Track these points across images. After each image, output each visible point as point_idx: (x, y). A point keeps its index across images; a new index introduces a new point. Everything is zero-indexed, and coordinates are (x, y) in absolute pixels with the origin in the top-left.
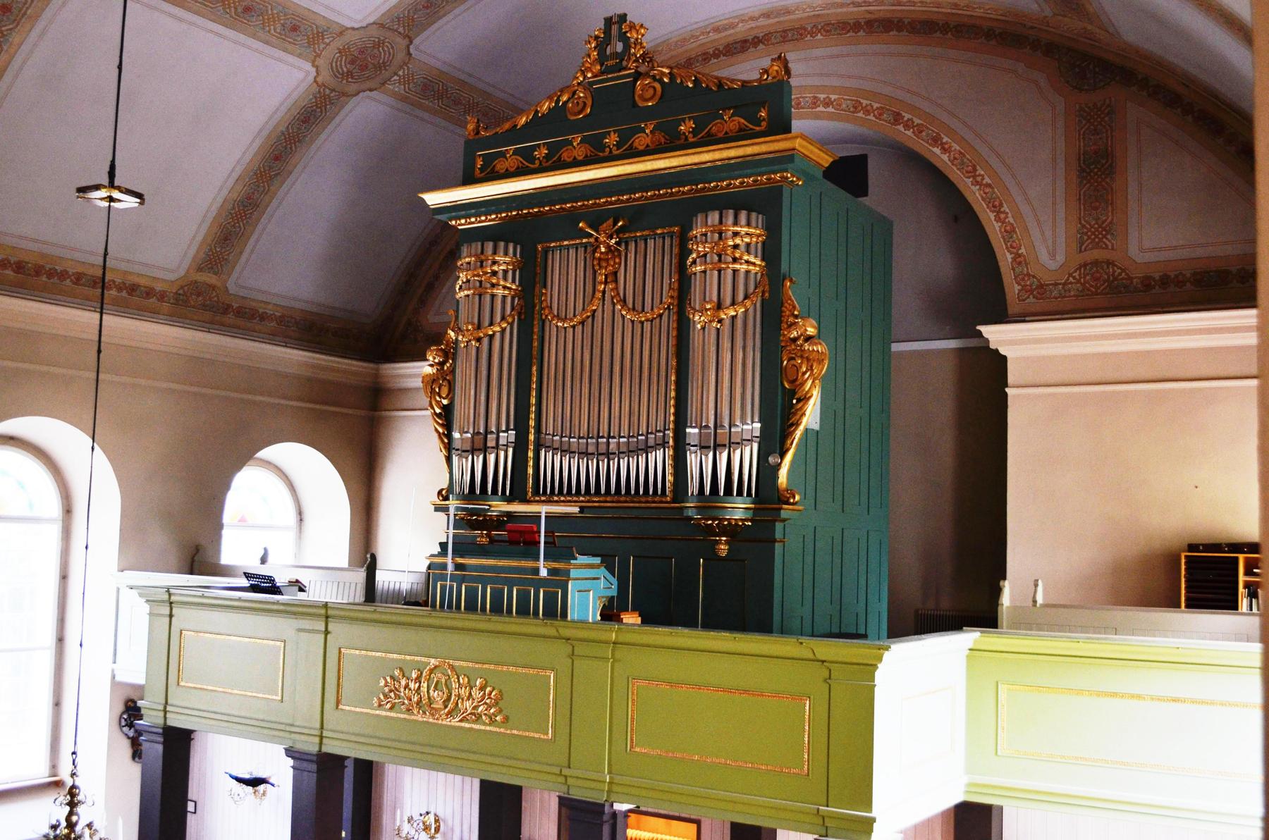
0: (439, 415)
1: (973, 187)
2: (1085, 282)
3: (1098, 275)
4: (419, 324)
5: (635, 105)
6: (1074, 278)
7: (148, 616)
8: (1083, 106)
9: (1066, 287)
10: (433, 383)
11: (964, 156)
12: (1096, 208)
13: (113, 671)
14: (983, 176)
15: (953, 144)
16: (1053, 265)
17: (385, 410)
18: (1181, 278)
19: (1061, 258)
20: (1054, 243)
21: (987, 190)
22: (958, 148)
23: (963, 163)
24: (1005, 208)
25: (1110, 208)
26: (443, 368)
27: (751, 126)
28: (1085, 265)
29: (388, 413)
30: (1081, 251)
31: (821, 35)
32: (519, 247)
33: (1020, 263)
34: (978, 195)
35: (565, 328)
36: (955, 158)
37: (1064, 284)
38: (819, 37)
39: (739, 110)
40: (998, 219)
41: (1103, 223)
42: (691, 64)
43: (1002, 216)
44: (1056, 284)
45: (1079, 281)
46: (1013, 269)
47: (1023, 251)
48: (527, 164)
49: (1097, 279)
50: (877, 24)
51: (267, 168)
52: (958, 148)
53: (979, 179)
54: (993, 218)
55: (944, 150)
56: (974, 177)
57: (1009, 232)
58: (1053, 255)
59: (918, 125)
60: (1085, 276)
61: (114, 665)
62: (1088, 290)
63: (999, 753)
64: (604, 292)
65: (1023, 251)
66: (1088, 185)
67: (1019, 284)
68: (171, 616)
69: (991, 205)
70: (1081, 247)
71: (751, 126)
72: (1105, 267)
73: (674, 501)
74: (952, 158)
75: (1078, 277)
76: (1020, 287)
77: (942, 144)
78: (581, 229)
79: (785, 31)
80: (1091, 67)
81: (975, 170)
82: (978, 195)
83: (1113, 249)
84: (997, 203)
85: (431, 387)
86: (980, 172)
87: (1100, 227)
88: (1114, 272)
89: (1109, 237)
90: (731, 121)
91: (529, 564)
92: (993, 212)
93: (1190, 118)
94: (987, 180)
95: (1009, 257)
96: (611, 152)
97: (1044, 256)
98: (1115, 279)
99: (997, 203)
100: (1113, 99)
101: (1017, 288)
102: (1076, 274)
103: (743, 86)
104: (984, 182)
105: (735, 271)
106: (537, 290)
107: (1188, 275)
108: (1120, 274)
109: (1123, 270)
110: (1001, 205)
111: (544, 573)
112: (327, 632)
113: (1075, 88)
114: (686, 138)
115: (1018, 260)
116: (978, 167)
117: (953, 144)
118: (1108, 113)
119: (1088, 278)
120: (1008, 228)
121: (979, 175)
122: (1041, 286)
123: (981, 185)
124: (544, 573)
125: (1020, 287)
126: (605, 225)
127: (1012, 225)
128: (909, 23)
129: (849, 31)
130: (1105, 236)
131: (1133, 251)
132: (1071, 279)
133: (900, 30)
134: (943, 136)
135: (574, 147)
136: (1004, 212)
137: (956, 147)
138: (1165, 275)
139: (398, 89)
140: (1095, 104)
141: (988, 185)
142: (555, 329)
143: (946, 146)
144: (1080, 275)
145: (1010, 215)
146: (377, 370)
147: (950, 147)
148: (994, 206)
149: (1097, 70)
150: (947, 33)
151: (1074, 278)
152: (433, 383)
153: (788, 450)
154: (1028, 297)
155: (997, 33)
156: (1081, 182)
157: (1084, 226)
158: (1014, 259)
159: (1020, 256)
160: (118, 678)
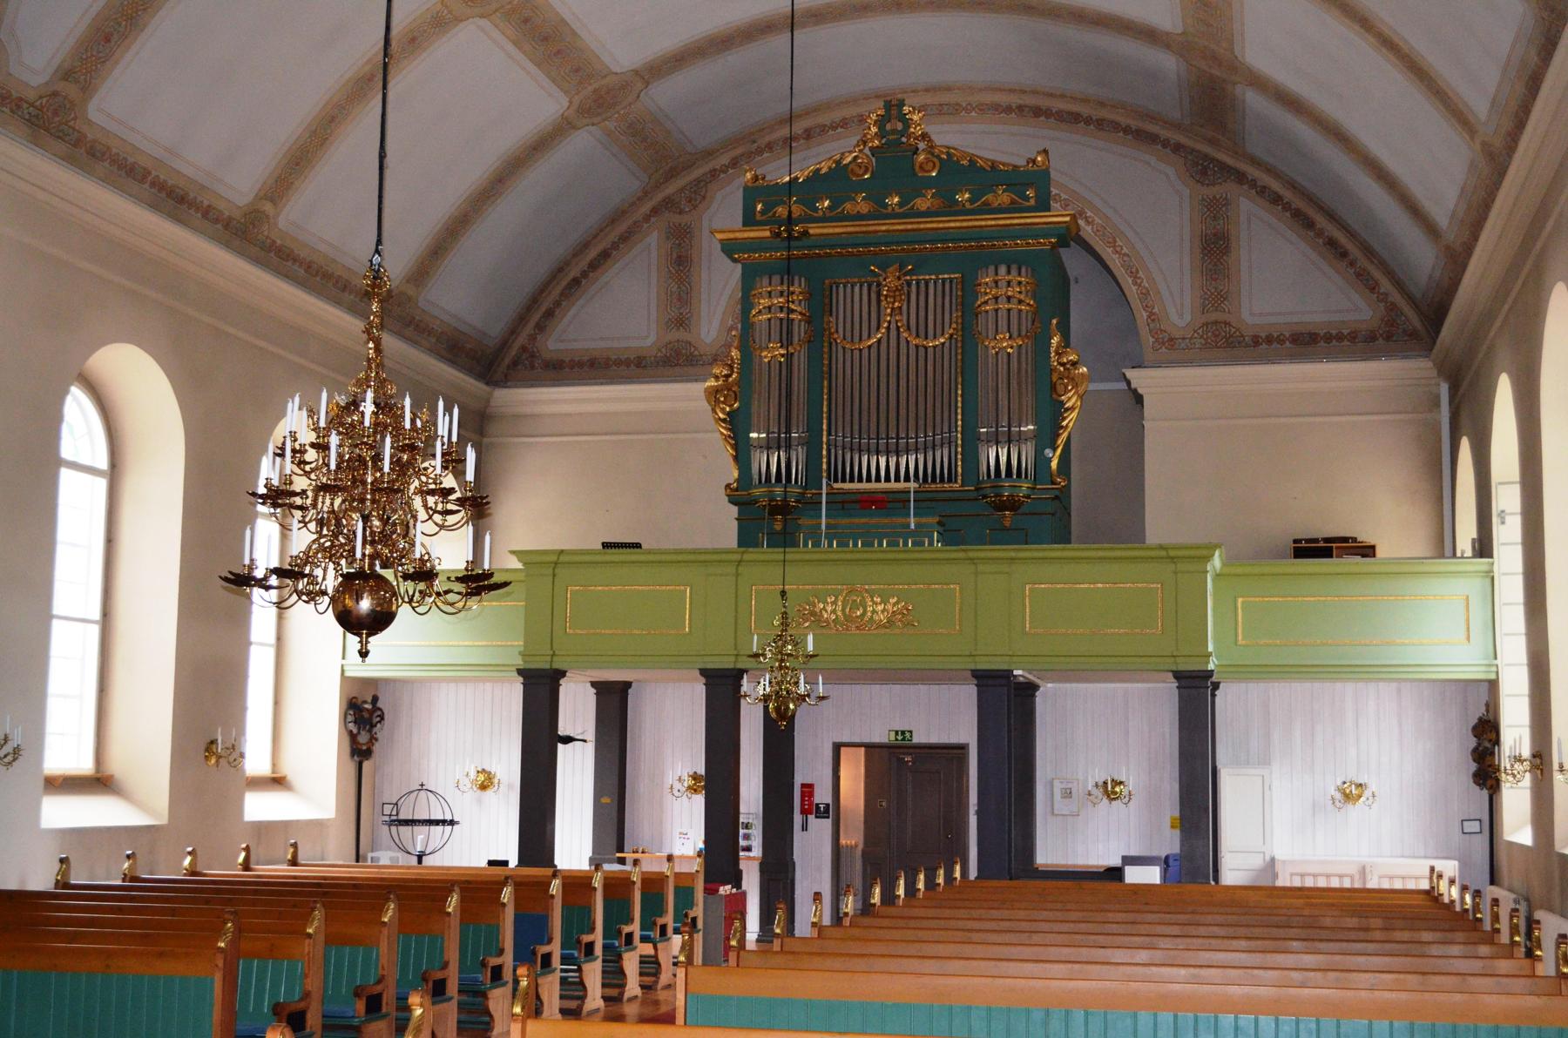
0: (724, 421)
1: (1114, 256)
2: (1208, 338)
3: (1217, 333)
4: (535, 350)
5: (915, 174)
6: (1198, 334)
7: (736, 522)
8: (1205, 197)
9: (1192, 341)
10: (716, 393)
11: (1105, 229)
12: (1215, 280)
13: (342, 666)
14: (1121, 247)
15: (1096, 218)
16: (1181, 323)
17: (511, 436)
18: (1282, 337)
19: (1188, 317)
20: (1182, 305)
21: (1125, 259)
22: (1100, 222)
23: (1104, 235)
24: (1141, 274)
25: (1227, 280)
26: (727, 381)
27: (1020, 201)
28: (1207, 324)
29: (501, 439)
30: (1203, 313)
31: (976, 112)
32: (803, 279)
33: (1153, 320)
34: (1117, 261)
35: (852, 350)
36: (1098, 231)
37: (1191, 338)
38: (973, 114)
39: (1010, 186)
40: (1135, 283)
41: (1221, 291)
42: (846, 124)
43: (1139, 281)
44: (1184, 339)
45: (1202, 337)
46: (1148, 325)
47: (1156, 310)
48: (809, 212)
49: (1216, 336)
50: (1027, 109)
51: (1218, 263)
52: (1100, 222)
53: (1118, 249)
54: (1130, 281)
55: (1088, 223)
56: (1114, 247)
57: (1145, 294)
58: (1181, 316)
59: (1065, 199)
60: (1207, 332)
61: (344, 662)
62: (1210, 344)
63: (1056, 812)
64: (889, 322)
65: (1156, 310)
66: (1209, 261)
67: (1153, 337)
68: (554, 575)
69: (1128, 271)
70: (1203, 309)
71: (1020, 201)
72: (1223, 326)
73: (962, 486)
74: (1095, 229)
75: (1201, 333)
76: (1154, 340)
77: (1086, 217)
78: (872, 271)
79: (941, 105)
80: (1211, 166)
81: (1115, 241)
82: (1117, 261)
83: (1229, 313)
84: (1134, 270)
85: (715, 397)
86: (1119, 243)
87: (1218, 294)
88: (1230, 330)
89: (1225, 302)
90: (1003, 197)
91: (900, 520)
92: (1131, 277)
93: (1288, 214)
94: (1125, 250)
95: (1145, 315)
96: (893, 209)
97: (1174, 317)
98: (1231, 336)
99: (1134, 270)
100: (1229, 194)
101: (1151, 340)
102: (1200, 331)
103: (1013, 169)
104: (1123, 252)
105: (1020, 311)
106: (826, 319)
107: (1287, 336)
108: (1235, 332)
109: (1238, 330)
110: (1137, 272)
111: (913, 526)
112: (737, 575)
113: (1198, 181)
114: (964, 205)
115: (1152, 318)
116: (1118, 239)
117: (1096, 218)
118: (1225, 205)
119: (1210, 334)
120: (1144, 291)
121: (1119, 246)
122: (1171, 339)
123: (1120, 254)
124: (913, 526)
125: (1154, 340)
126: (891, 268)
127: (1147, 288)
128: (1056, 112)
129: (1001, 112)
130: (1222, 302)
131: (1245, 315)
132: (1196, 335)
133: (1048, 117)
134: (1086, 210)
135: (858, 203)
136: (1139, 278)
137: (1097, 220)
138: (1270, 334)
139: (611, 125)
140: (1215, 197)
141: (1125, 255)
142: (842, 351)
143: (1090, 220)
144: (1203, 332)
145: (1145, 281)
146: (491, 394)
147: (1093, 221)
148: (1131, 272)
149: (1216, 169)
150: (1090, 124)
151: (1198, 334)
152: (716, 393)
153: (1058, 447)
154: (1161, 348)
155: (1133, 130)
156: (1203, 258)
157: (1206, 293)
158: (1149, 317)
159: (1154, 314)
160: (348, 674)
